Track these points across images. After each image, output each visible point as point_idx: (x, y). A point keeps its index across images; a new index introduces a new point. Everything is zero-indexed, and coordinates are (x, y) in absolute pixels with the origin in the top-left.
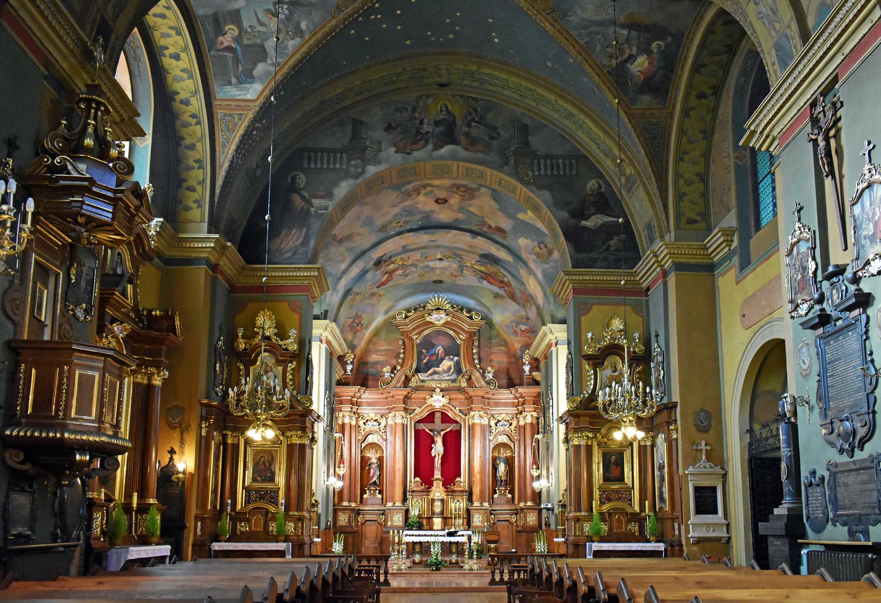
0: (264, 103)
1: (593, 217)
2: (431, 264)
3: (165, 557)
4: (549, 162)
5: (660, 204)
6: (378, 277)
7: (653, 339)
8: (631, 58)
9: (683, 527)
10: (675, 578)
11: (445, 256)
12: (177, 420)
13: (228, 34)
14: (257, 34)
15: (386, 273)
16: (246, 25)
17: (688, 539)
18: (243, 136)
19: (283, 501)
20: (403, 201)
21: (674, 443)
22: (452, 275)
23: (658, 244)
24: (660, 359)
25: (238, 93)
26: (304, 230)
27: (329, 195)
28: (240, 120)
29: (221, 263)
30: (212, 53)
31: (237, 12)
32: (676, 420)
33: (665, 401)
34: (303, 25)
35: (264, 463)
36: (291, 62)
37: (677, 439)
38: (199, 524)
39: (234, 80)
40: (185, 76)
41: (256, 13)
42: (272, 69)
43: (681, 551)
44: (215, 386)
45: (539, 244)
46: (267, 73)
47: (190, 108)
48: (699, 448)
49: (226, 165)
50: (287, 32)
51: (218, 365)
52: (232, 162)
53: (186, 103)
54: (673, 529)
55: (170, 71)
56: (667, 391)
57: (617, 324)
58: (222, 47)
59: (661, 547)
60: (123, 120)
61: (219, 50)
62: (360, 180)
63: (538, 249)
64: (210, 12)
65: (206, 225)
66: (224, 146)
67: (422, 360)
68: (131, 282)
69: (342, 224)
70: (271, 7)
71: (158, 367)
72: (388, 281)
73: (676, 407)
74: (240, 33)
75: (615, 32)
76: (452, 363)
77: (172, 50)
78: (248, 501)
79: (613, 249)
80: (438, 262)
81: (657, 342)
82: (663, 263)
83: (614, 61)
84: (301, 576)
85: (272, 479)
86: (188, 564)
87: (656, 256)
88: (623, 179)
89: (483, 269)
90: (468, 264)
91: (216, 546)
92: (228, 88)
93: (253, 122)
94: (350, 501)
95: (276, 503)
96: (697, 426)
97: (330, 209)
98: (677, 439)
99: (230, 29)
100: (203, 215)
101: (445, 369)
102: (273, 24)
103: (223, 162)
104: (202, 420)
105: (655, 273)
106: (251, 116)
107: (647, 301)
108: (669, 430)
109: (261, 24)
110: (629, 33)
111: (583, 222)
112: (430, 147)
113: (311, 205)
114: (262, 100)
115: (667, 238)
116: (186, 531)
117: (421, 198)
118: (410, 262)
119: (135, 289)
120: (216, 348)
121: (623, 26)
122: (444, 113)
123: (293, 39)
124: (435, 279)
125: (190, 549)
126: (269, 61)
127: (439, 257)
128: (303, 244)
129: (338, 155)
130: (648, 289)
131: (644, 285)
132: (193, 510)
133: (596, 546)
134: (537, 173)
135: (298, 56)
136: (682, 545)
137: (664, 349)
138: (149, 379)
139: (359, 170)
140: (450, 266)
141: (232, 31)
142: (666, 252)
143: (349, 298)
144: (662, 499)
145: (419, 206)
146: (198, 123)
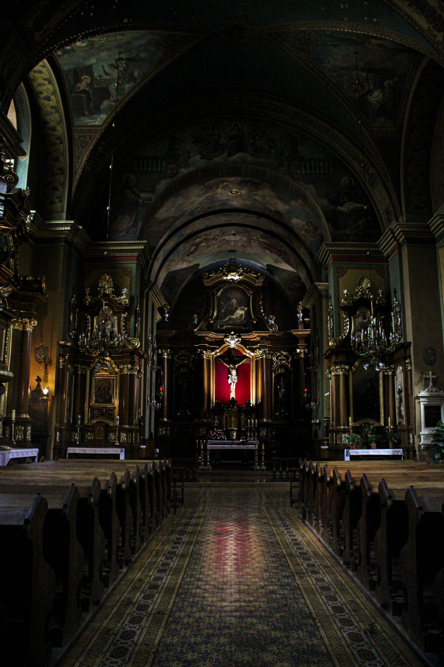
0: (107, 128)
1: (347, 204)
2: (227, 238)
3: (34, 457)
4: (312, 164)
5: (395, 195)
6: (188, 248)
7: (393, 294)
8: (370, 92)
9: (416, 437)
10: (404, 474)
11: (238, 232)
12: (43, 356)
13: (84, 82)
14: (103, 81)
15: (194, 245)
16: (96, 75)
17: (420, 446)
18: (92, 150)
19: (118, 417)
20: (208, 192)
21: (409, 373)
22: (243, 246)
23: (393, 224)
24: (398, 309)
25: (89, 121)
26: (135, 215)
27: (152, 190)
28: (90, 139)
29: (75, 241)
30: (73, 95)
31: (91, 66)
32: (410, 356)
33: (402, 341)
34: (136, 74)
35: (104, 389)
36: (127, 99)
37: (411, 370)
38: (58, 434)
39: (87, 113)
40: (54, 111)
41: (103, 67)
42: (113, 104)
43: (415, 455)
44: (69, 331)
45: (307, 223)
46: (110, 107)
47: (56, 133)
48: (428, 377)
49: (80, 171)
50: (125, 79)
51: (71, 316)
52: (84, 169)
53: (54, 129)
54: (409, 438)
55: (44, 108)
56: (404, 334)
57: (366, 284)
58: (79, 90)
59: (400, 452)
60: (11, 145)
61: (77, 93)
62: (175, 179)
63: (306, 226)
64: (71, 67)
65: (65, 214)
66: (79, 157)
67: (220, 310)
68: (13, 257)
69: (162, 211)
70: (114, 62)
71: (30, 318)
72: (195, 250)
73: (410, 346)
74: (92, 81)
75: (357, 74)
76: (243, 312)
77: (45, 94)
78: (93, 417)
79: (361, 227)
80: (232, 237)
81: (396, 297)
82: (398, 238)
83: (357, 94)
84: (132, 472)
85: (110, 401)
86: (51, 462)
87: (393, 233)
88: (367, 177)
89: (266, 241)
90: (254, 238)
91: (71, 450)
92: (82, 118)
93: (99, 140)
94: (344, 426)
95: (113, 419)
96: (425, 360)
97: (153, 200)
98: (411, 370)
99: (85, 78)
100: (62, 207)
101: (238, 316)
102: (115, 74)
103: (78, 169)
104: (60, 357)
105: (393, 245)
106: (98, 136)
107: (388, 267)
108: (405, 363)
109: (106, 74)
110: (368, 75)
111: (339, 207)
112: (225, 154)
113: (140, 197)
114: (105, 125)
115: (400, 219)
116: (49, 439)
117: (219, 190)
118: (212, 236)
119: (15, 262)
120: (70, 303)
121: (363, 70)
122: (236, 130)
123: (128, 83)
124: (230, 248)
125: (52, 452)
126: (112, 99)
127: (233, 232)
128: (133, 226)
129: (159, 161)
130: (388, 257)
131: (385, 254)
132: (54, 423)
133: (354, 452)
134: (304, 172)
135: (132, 94)
136: (415, 451)
137: (400, 302)
138: (24, 327)
139: (174, 172)
140: (241, 239)
141: (86, 79)
142: (400, 229)
143: (167, 264)
144: (401, 416)
145: (218, 196)
146: (62, 143)
